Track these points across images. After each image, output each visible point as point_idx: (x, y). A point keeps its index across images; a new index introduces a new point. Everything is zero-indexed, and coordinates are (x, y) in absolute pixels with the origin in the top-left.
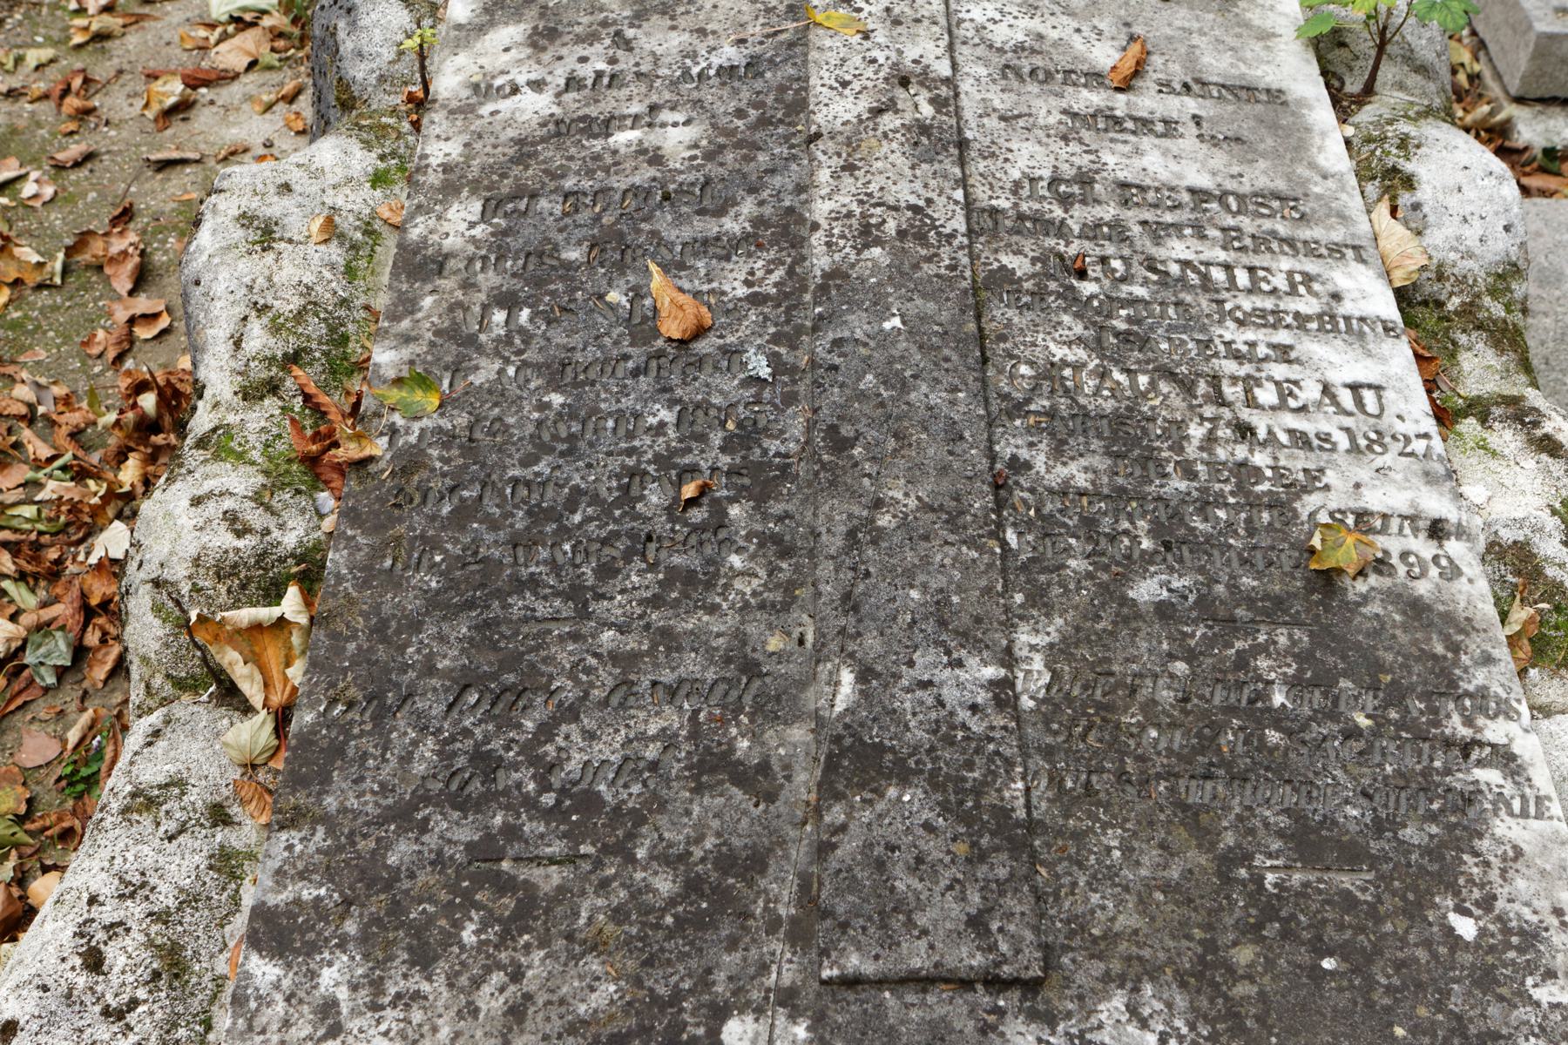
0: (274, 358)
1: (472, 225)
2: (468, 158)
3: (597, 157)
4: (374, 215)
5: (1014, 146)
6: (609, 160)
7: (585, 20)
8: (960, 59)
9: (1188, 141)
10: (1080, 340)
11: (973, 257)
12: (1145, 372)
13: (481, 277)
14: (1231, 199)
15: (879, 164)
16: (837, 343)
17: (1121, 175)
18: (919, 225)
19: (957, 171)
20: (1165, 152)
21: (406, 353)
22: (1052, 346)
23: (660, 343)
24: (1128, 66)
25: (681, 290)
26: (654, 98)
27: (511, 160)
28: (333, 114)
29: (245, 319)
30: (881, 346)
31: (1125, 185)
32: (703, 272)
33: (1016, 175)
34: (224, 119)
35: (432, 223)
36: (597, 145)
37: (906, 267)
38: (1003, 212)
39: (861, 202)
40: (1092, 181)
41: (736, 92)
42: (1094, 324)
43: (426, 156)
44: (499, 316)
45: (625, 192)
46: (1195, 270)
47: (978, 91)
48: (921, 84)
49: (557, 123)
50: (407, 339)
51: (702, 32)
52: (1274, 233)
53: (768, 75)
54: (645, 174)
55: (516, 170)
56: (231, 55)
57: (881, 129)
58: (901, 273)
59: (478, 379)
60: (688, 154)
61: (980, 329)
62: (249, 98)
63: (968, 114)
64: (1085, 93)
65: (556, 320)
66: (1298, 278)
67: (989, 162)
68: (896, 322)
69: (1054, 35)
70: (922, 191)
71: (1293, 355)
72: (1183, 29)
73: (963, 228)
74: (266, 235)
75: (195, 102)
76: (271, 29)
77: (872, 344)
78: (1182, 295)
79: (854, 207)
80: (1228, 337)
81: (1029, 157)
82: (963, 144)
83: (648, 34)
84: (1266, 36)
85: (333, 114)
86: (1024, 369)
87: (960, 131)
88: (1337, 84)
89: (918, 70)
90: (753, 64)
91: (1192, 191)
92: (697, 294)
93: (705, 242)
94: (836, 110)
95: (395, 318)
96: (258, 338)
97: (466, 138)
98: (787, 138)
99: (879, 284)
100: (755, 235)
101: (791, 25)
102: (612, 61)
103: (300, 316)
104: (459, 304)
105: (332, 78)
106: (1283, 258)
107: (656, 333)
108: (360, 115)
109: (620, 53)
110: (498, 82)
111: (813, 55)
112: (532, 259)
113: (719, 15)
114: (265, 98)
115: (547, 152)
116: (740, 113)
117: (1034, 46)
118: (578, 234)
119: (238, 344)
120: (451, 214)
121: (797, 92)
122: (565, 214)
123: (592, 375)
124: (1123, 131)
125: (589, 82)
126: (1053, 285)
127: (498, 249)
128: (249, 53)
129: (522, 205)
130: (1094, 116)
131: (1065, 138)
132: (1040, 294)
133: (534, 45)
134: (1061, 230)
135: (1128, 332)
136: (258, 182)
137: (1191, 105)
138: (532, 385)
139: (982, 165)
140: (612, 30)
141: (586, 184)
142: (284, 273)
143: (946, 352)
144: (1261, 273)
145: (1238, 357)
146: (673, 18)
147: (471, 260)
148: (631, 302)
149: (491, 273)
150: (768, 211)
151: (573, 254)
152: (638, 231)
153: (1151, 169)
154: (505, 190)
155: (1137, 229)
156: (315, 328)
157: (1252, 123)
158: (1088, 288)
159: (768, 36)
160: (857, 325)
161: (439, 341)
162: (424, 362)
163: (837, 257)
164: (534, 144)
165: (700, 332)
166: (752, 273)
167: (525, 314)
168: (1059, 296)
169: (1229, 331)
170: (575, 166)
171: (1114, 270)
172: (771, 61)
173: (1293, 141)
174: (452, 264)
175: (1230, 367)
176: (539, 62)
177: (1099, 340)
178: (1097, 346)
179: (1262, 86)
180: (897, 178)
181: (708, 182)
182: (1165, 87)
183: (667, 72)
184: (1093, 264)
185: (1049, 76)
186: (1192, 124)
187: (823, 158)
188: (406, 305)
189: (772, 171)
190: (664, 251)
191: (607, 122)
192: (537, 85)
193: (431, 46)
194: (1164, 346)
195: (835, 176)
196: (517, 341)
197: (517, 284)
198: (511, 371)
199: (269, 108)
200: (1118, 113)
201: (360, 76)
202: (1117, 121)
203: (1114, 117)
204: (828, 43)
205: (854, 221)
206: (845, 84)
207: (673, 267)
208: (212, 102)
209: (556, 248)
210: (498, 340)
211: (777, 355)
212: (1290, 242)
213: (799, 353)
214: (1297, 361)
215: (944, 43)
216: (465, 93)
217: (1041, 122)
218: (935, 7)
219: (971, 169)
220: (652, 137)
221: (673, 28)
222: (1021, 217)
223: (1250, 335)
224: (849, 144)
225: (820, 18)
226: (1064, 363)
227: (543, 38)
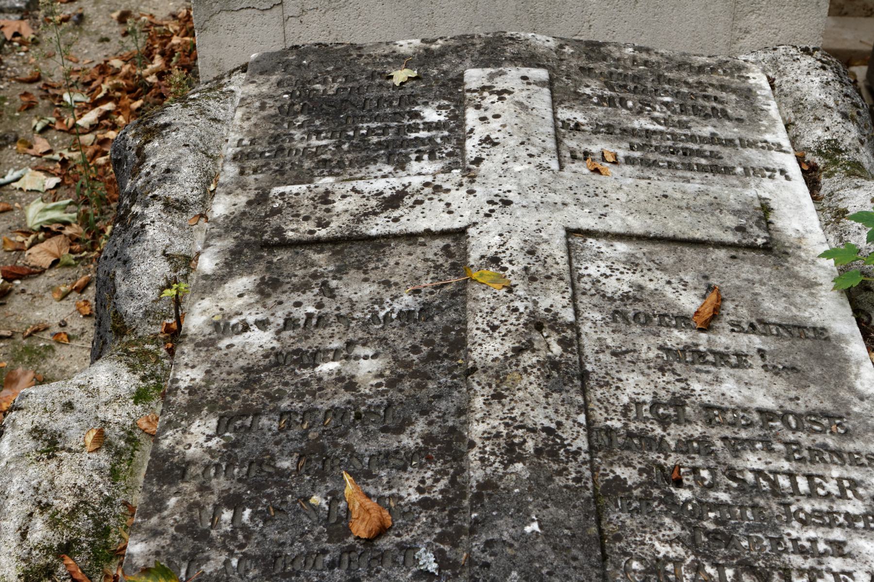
0: (51, 548)
1: (209, 438)
2: (208, 382)
3: (306, 383)
4: (135, 426)
5: (624, 377)
6: (315, 386)
7: (300, 273)
8: (581, 307)
9: (755, 372)
10: (678, 540)
11: (594, 469)
12: (730, 566)
13: (214, 481)
14: (791, 418)
15: (520, 394)
16: (489, 544)
17: (705, 399)
18: (552, 446)
19: (580, 399)
20: (739, 380)
21: (153, 545)
22: (657, 544)
23: (351, 540)
24: (708, 311)
25: (368, 496)
26: (351, 336)
27: (241, 385)
28: (109, 337)
29: (31, 515)
30: (523, 547)
31: (708, 407)
32: (385, 480)
33: (625, 400)
34: (32, 304)
35: (178, 435)
36: (306, 373)
37: (542, 480)
38: (616, 430)
39: (507, 425)
40: (684, 404)
41: (412, 332)
42: (689, 524)
43: (175, 381)
44: (227, 515)
45: (327, 412)
46: (767, 479)
47: (595, 332)
48: (552, 328)
49: (277, 355)
50: (155, 533)
51: (387, 284)
52: (825, 446)
53: (437, 318)
54: (342, 398)
55: (245, 393)
56: (39, 256)
57: (522, 365)
58: (538, 484)
59: (208, 568)
60: (374, 382)
61: (601, 531)
62: (51, 288)
63: (589, 350)
64: (676, 332)
65: (272, 519)
66: (846, 484)
67: (604, 390)
68: (535, 526)
69: (651, 286)
70: (553, 416)
71: (846, 550)
72: (748, 280)
73: (585, 447)
74: (50, 444)
75: (11, 291)
76: (71, 236)
77: (516, 545)
78: (757, 500)
79: (502, 428)
80: (794, 535)
81: (634, 385)
82: (584, 376)
83: (347, 285)
84: (810, 285)
85: (109, 337)
86: (635, 565)
87: (582, 365)
88: (866, 319)
89: (550, 317)
90: (425, 308)
91: (760, 411)
92: (380, 499)
93: (387, 455)
94: (488, 349)
95: (146, 515)
96: (39, 532)
97: (207, 366)
98: (450, 370)
99: (521, 494)
100: (426, 449)
101: (453, 280)
102: (320, 306)
103: (73, 513)
104: (197, 505)
105: (110, 310)
106: (834, 467)
107: (348, 532)
108: (129, 343)
109: (325, 299)
110: (234, 321)
111: (471, 304)
112: (254, 466)
113: (400, 270)
114: (63, 289)
115: (268, 378)
116: (415, 349)
117: (637, 295)
118: (290, 446)
119: (24, 535)
120: (194, 428)
121: (458, 332)
122: (281, 430)
123: (298, 567)
124: (706, 363)
125: (302, 322)
126: (656, 492)
127: (228, 457)
128: (53, 254)
129: (248, 423)
130: (683, 351)
131: (662, 370)
132: (646, 499)
133: (261, 292)
134: (660, 445)
135: (716, 532)
136: (48, 401)
137: (757, 341)
138: (251, 575)
139: (599, 392)
140: (320, 281)
141: (298, 405)
142: (63, 477)
143: (574, 552)
144: (818, 480)
145: (802, 552)
146: (365, 272)
147: (207, 467)
148: (329, 504)
149: (222, 479)
150: (435, 429)
151: (285, 464)
152: (336, 445)
153: (729, 394)
154: (235, 409)
155: (719, 444)
156: (84, 523)
157: (803, 355)
158: (684, 494)
159: (436, 288)
160: (505, 529)
161: (180, 535)
162: (168, 553)
163: (489, 470)
164: (259, 372)
165: (383, 531)
166: (423, 481)
167: (247, 513)
168: (661, 501)
169: (795, 531)
170: (289, 390)
171: (703, 479)
172: (438, 307)
173: (835, 370)
174: (192, 470)
175: (797, 560)
176: (264, 306)
177: (693, 539)
178: (691, 544)
179: (809, 325)
180: (534, 405)
181: (390, 404)
182: (736, 327)
183: (360, 315)
184: (687, 473)
185: (648, 319)
186: (757, 357)
187: (478, 388)
188: (156, 504)
189: (439, 397)
190: (355, 461)
191: (314, 355)
192: (263, 325)
193: (184, 293)
194: (745, 543)
195: (487, 403)
196: (240, 537)
197: (241, 488)
198: (234, 562)
199: (65, 296)
200: (701, 348)
201: (131, 311)
202: (701, 355)
203: (698, 352)
204: (481, 295)
205: (501, 441)
206: (494, 328)
207: (362, 476)
208: (23, 291)
209: (273, 458)
210: (225, 535)
211: (442, 551)
212: (838, 453)
213: (459, 550)
214: (850, 555)
215: (568, 295)
216: (208, 330)
217: (643, 356)
218: (561, 266)
219: (591, 396)
220: (348, 368)
221: (366, 280)
222: (630, 435)
223: (812, 534)
224: (497, 377)
225: (475, 275)
226: (667, 559)
227: (267, 288)
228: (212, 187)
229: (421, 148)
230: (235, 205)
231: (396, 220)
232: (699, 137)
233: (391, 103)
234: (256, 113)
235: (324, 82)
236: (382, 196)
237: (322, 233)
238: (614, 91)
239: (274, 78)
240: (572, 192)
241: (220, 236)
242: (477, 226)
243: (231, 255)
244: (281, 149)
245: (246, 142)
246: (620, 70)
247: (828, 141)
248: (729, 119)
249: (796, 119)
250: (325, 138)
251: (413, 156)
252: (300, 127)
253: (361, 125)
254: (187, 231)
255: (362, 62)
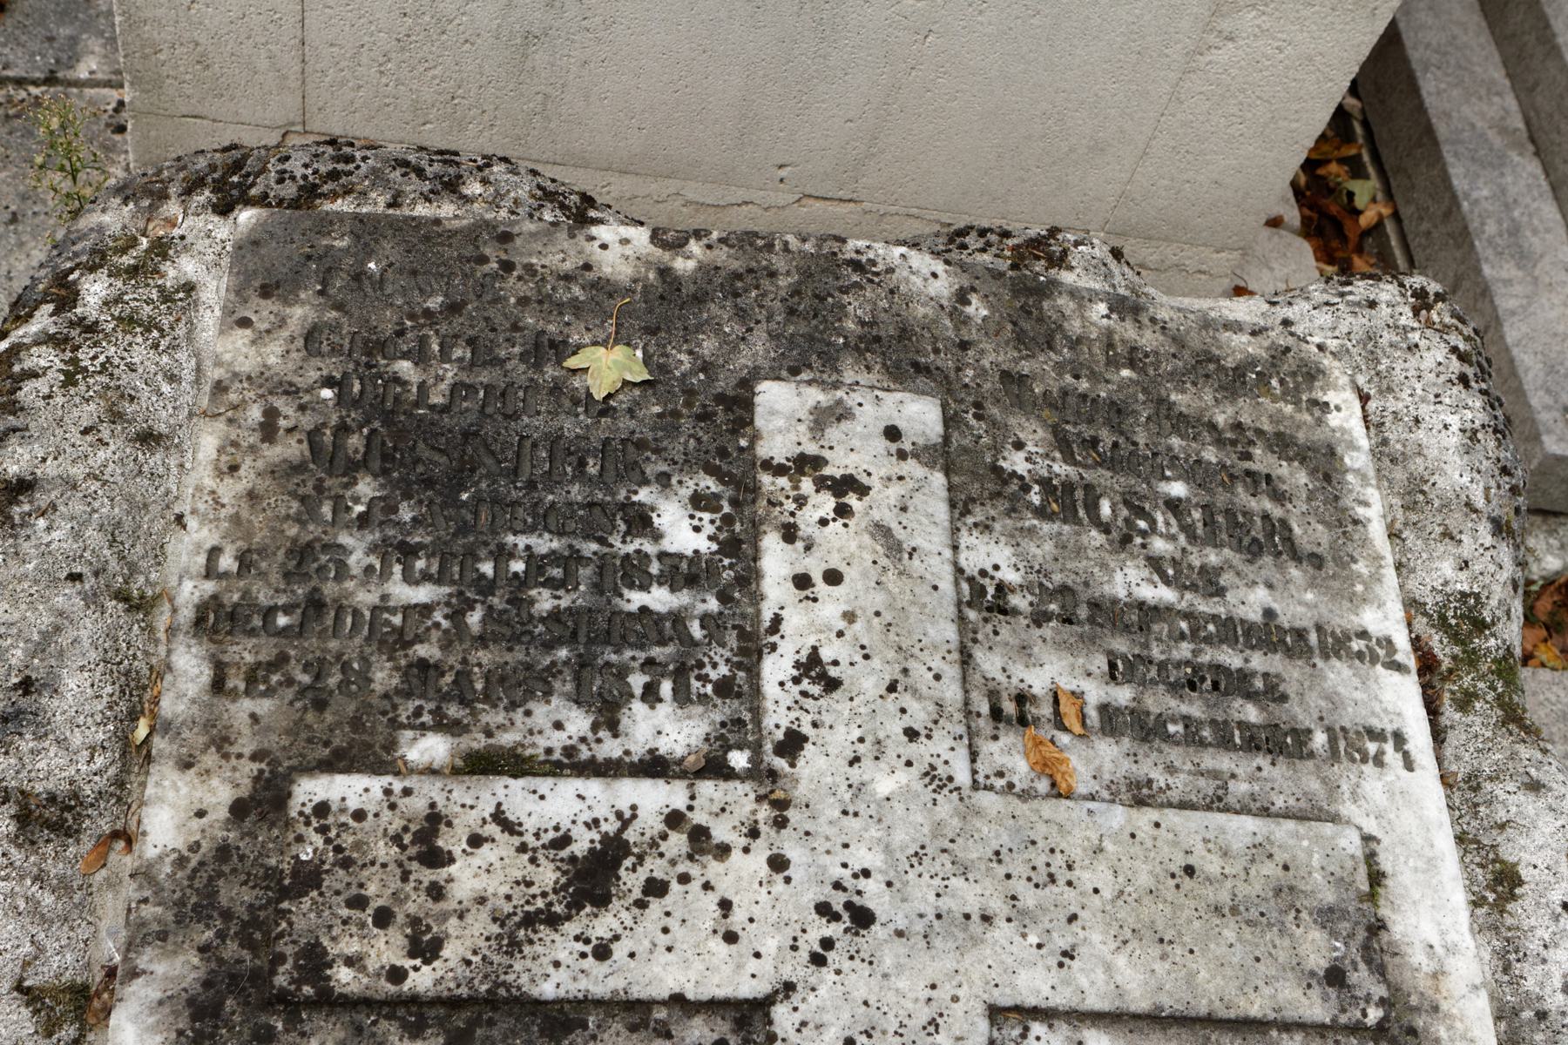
228: (142, 731)
229: (657, 652)
230: (201, 814)
231: (602, 952)
232: (1242, 621)
233: (582, 464)
234: (252, 449)
235: (420, 356)
236: (564, 853)
237: (422, 979)
238: (1075, 463)
239: (300, 314)
240: (1001, 871)
241: (163, 936)
242: (796, 999)
243: (194, 1018)
244: (315, 604)
245: (227, 562)
246: (1084, 385)
247: (1464, 595)
248: (1296, 557)
249: (1406, 524)
250: (426, 577)
251: (637, 681)
252: (363, 521)
253: (510, 539)
254: (77, 898)
255: (513, 288)
